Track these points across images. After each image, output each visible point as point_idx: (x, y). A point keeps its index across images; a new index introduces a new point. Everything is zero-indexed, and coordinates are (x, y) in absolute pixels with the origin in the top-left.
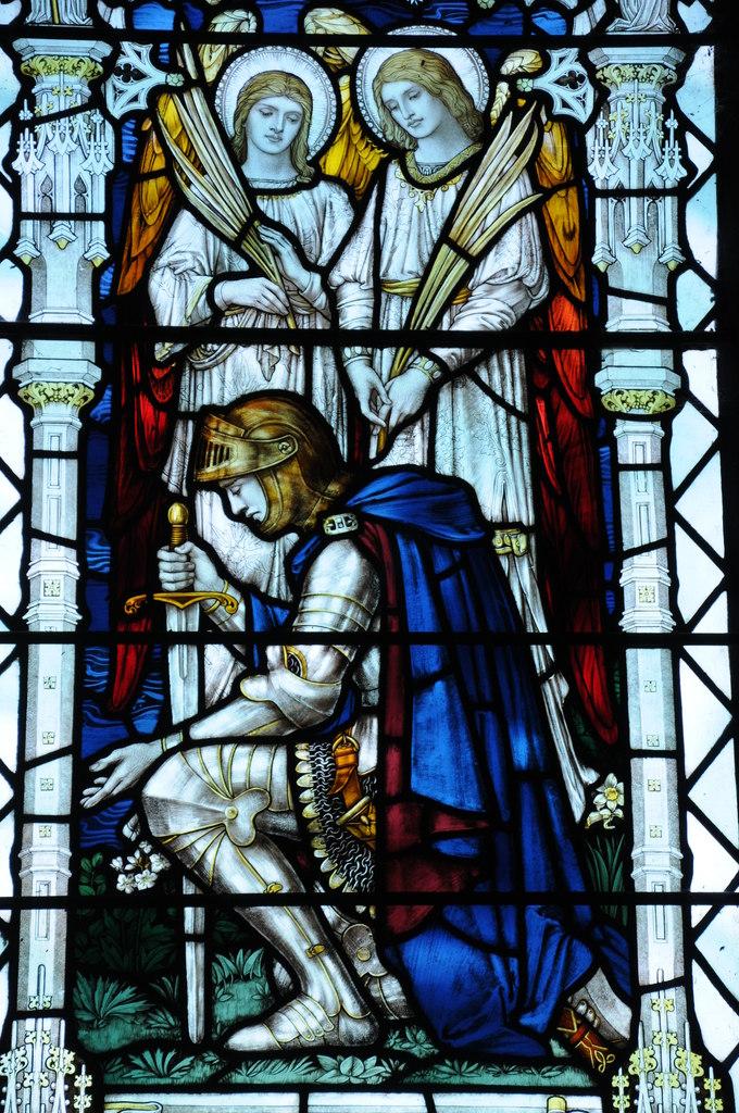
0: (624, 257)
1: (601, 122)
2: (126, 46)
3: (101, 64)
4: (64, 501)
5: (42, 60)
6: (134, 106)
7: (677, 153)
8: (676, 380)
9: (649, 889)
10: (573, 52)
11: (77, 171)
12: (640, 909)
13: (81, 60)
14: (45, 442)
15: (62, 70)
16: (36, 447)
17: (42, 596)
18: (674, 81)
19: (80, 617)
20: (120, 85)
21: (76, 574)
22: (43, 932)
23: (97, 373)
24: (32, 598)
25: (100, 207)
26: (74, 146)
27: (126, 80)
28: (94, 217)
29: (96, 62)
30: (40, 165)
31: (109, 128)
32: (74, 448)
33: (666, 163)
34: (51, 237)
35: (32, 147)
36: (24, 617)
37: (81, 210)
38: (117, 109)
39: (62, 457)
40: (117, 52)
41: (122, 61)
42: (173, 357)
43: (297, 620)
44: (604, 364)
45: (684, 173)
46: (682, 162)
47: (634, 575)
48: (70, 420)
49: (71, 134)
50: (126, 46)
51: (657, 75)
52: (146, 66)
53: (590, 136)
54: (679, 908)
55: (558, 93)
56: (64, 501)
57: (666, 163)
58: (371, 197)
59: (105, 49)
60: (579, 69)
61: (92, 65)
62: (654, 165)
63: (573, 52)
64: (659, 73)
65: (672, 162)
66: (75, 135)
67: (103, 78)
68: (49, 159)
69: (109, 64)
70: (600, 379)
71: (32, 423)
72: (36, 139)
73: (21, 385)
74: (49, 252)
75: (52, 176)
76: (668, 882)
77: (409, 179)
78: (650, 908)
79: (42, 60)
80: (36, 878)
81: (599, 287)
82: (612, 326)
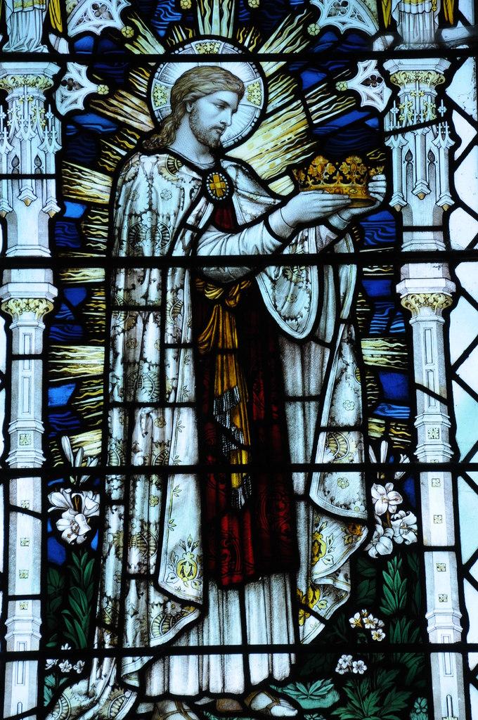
0: (413, 202)
1: (394, 110)
2: (70, 65)
3: (444, 75)
4: (33, 380)
5: (12, 78)
6: (74, 107)
7: (447, 130)
8: (452, 286)
9: (440, 641)
10: (374, 63)
11: (35, 152)
12: (433, 655)
13: (429, 73)
14: (21, 347)
15: (26, 84)
16: (10, 593)
17: (19, 446)
18: (444, 81)
19: (45, 460)
20: (67, 93)
21: (41, 429)
22: (26, 409)
23: (54, 292)
24: (11, 448)
25: (52, 171)
26: (34, 134)
27: (70, 89)
28: (49, 177)
29: (440, 74)
30: (10, 148)
31: (58, 122)
32: (40, 352)
33: (440, 136)
34: (20, 198)
35: (5, 136)
36: (7, 461)
37: (38, 172)
38: (63, 110)
39: (28, 355)
40: (64, 70)
41: (67, 76)
42: (277, 697)
43: (5, 46)
44: (402, 277)
45: (453, 143)
46: (450, 136)
47: (425, 420)
48: (36, 323)
49: (32, 127)
50: (70, 65)
51: (41, 82)
52: (84, 80)
53: (387, 119)
54: (460, 656)
55: (363, 91)
56: (33, 380)
57: (440, 136)
58: (105, 114)
59: (54, 69)
60: (377, 73)
61: (438, 76)
62: (432, 137)
63: (374, 63)
64: (433, 77)
65: (443, 135)
66: (35, 126)
67: (54, 89)
68: (16, 143)
69: (58, 79)
70: (399, 288)
71: (11, 327)
72: (8, 130)
73: (2, 301)
74: (19, 208)
75: (19, 155)
76: (453, 637)
77: (193, 130)
78: (440, 654)
79: (12, 78)
80: (17, 639)
81: (397, 223)
82: (407, 248)
